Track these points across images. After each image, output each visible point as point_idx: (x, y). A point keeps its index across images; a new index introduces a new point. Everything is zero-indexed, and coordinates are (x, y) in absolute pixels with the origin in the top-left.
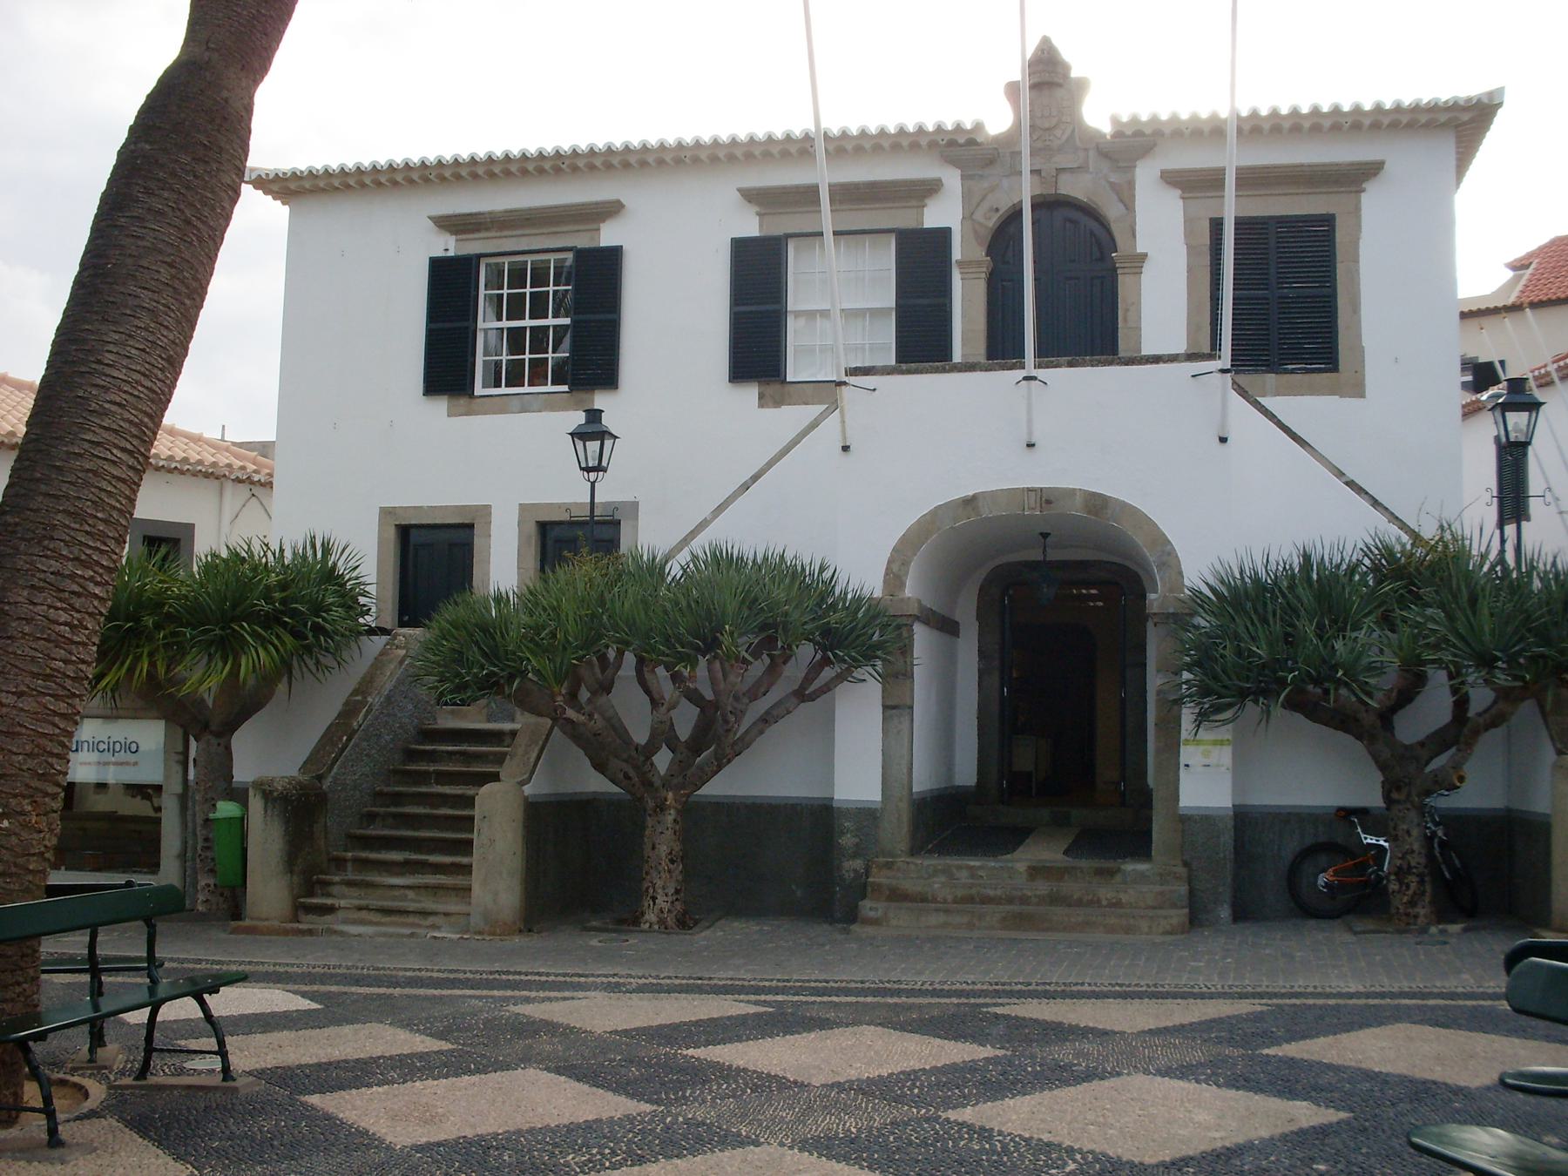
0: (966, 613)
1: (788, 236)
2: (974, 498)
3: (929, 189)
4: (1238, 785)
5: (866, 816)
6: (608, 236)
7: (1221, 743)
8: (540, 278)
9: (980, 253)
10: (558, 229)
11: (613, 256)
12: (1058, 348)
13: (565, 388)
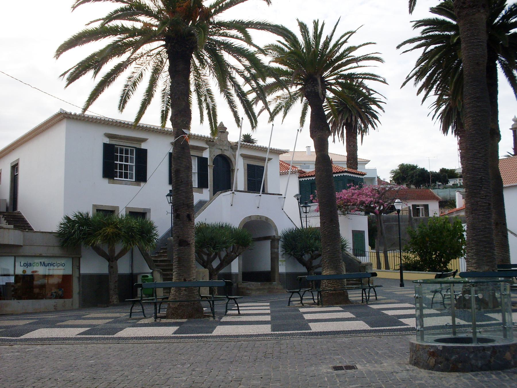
3: (203, 149)
5: (237, 275)
6: (143, 146)
8: (127, 152)
9: (212, 164)
10: (134, 142)
11: (145, 151)
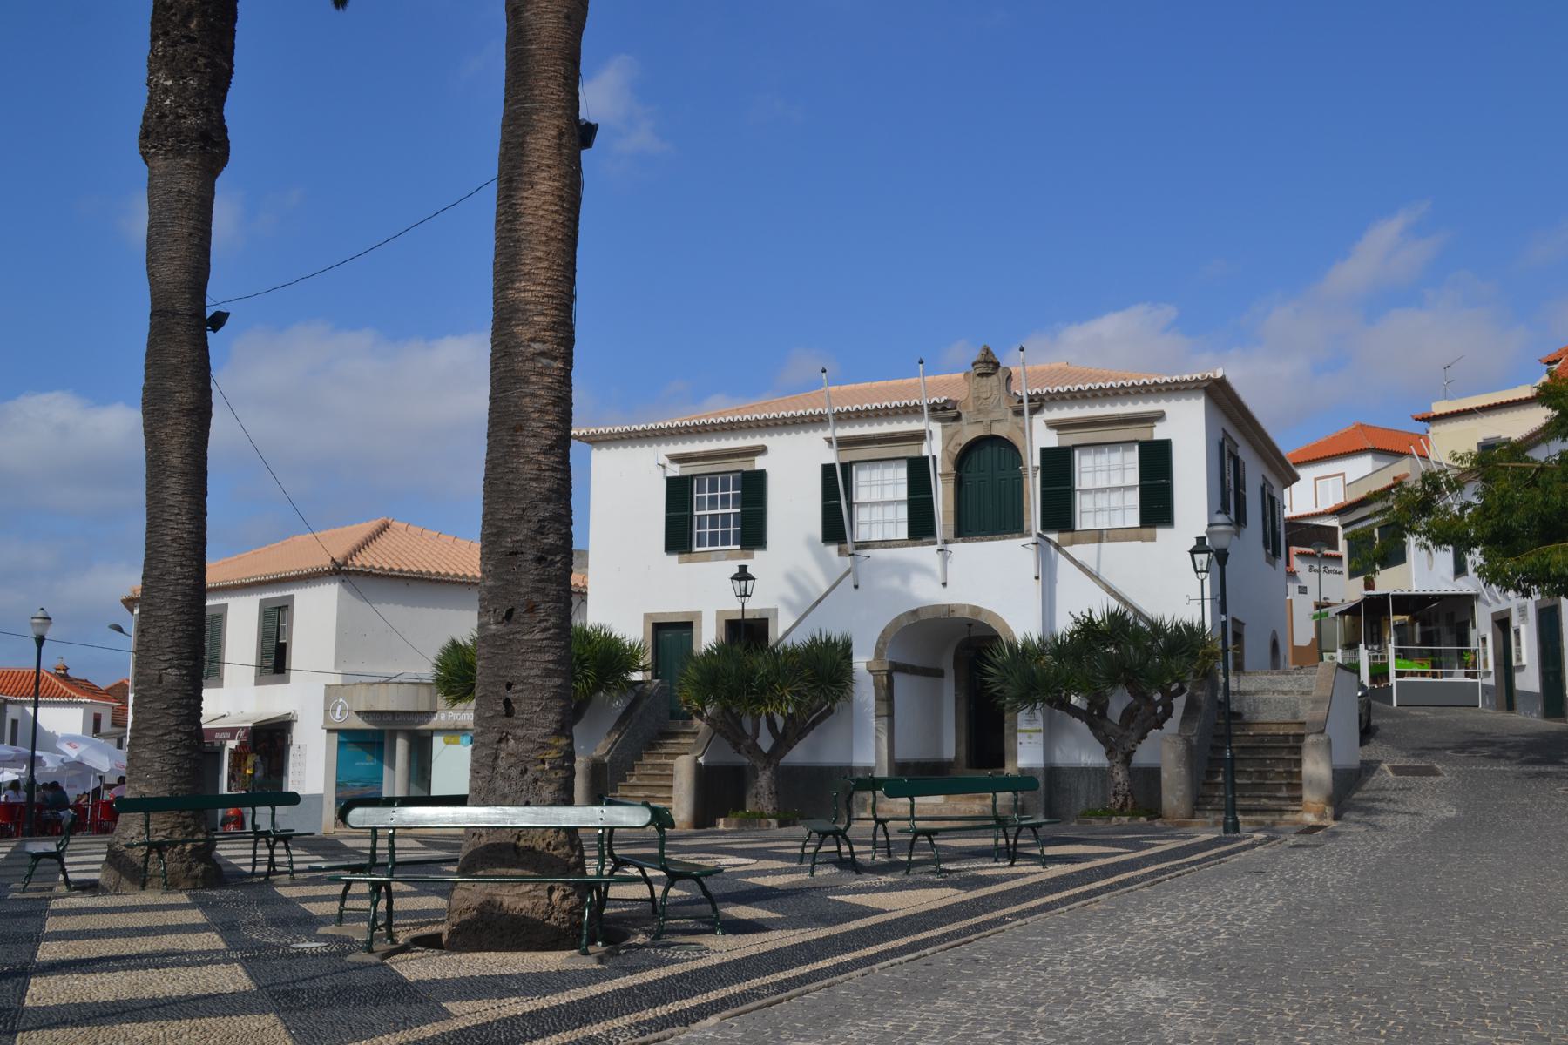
0: (947, 664)
1: (1075, 447)
2: (917, 610)
4: (1048, 751)
6: (759, 463)
7: (1036, 731)
9: (950, 468)
11: (1165, 445)
12: (966, 528)
13: (738, 547)
